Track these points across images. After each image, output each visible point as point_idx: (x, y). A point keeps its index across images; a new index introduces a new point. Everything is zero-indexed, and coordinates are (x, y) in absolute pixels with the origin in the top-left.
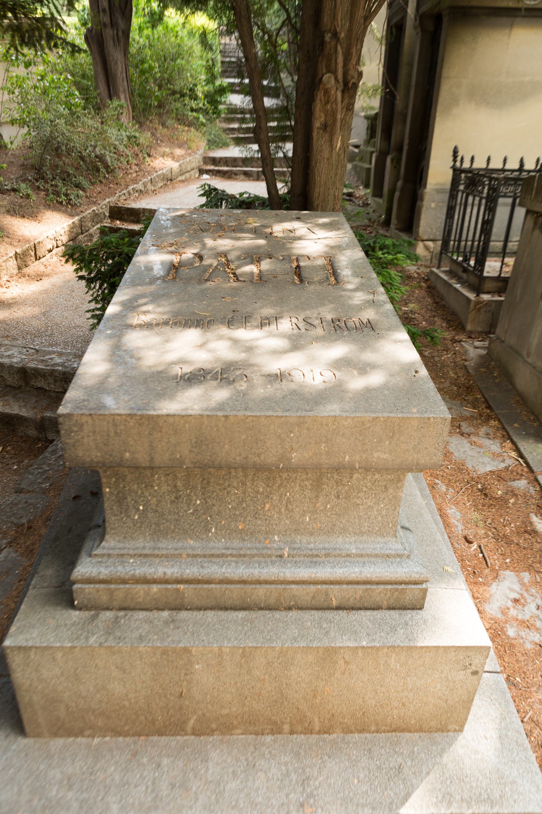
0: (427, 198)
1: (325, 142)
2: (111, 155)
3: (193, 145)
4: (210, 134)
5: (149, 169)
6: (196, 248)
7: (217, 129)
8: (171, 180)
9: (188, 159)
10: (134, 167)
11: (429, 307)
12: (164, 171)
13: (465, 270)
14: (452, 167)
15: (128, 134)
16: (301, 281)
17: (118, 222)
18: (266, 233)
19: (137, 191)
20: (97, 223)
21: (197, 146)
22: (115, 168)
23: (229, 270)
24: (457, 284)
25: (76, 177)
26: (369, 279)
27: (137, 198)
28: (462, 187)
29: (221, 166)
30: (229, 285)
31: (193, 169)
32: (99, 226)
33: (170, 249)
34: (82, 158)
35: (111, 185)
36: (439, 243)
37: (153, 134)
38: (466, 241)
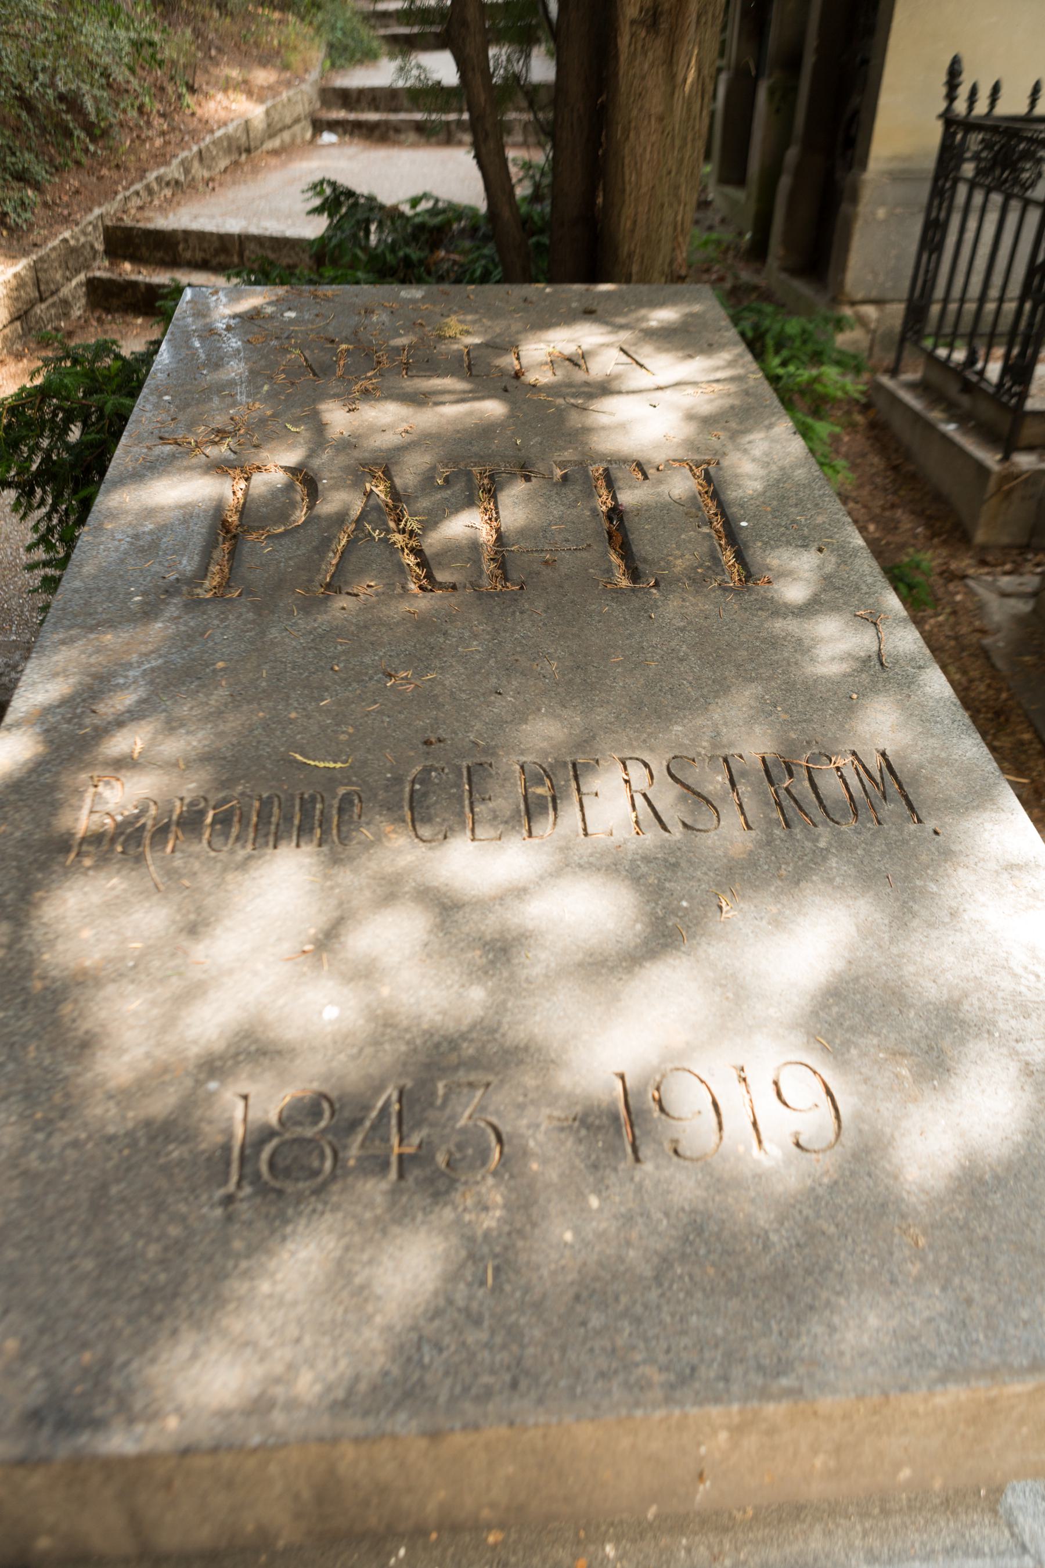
0: (867, 195)
1: (652, 65)
2: (97, 92)
3: (294, 59)
4: (333, 28)
5: (194, 123)
6: (292, 447)
7: (348, 14)
8: (248, 151)
9: (285, 96)
10: (157, 121)
11: (878, 480)
12: (231, 128)
13: (968, 387)
14: (940, 116)
15: (133, 35)
16: (635, 575)
17: (127, 266)
18: (502, 372)
19: (168, 184)
20: (77, 271)
21: (304, 61)
22: (111, 126)
23: (398, 538)
24: (949, 421)
25: (14, 154)
26: (845, 555)
27: (169, 201)
28: (968, 169)
29: (363, 111)
30: (405, 607)
31: (297, 121)
32: (82, 277)
33: (212, 451)
34: (25, 103)
35: (104, 172)
36: (898, 310)
37: (197, 33)
38: (962, 300)
